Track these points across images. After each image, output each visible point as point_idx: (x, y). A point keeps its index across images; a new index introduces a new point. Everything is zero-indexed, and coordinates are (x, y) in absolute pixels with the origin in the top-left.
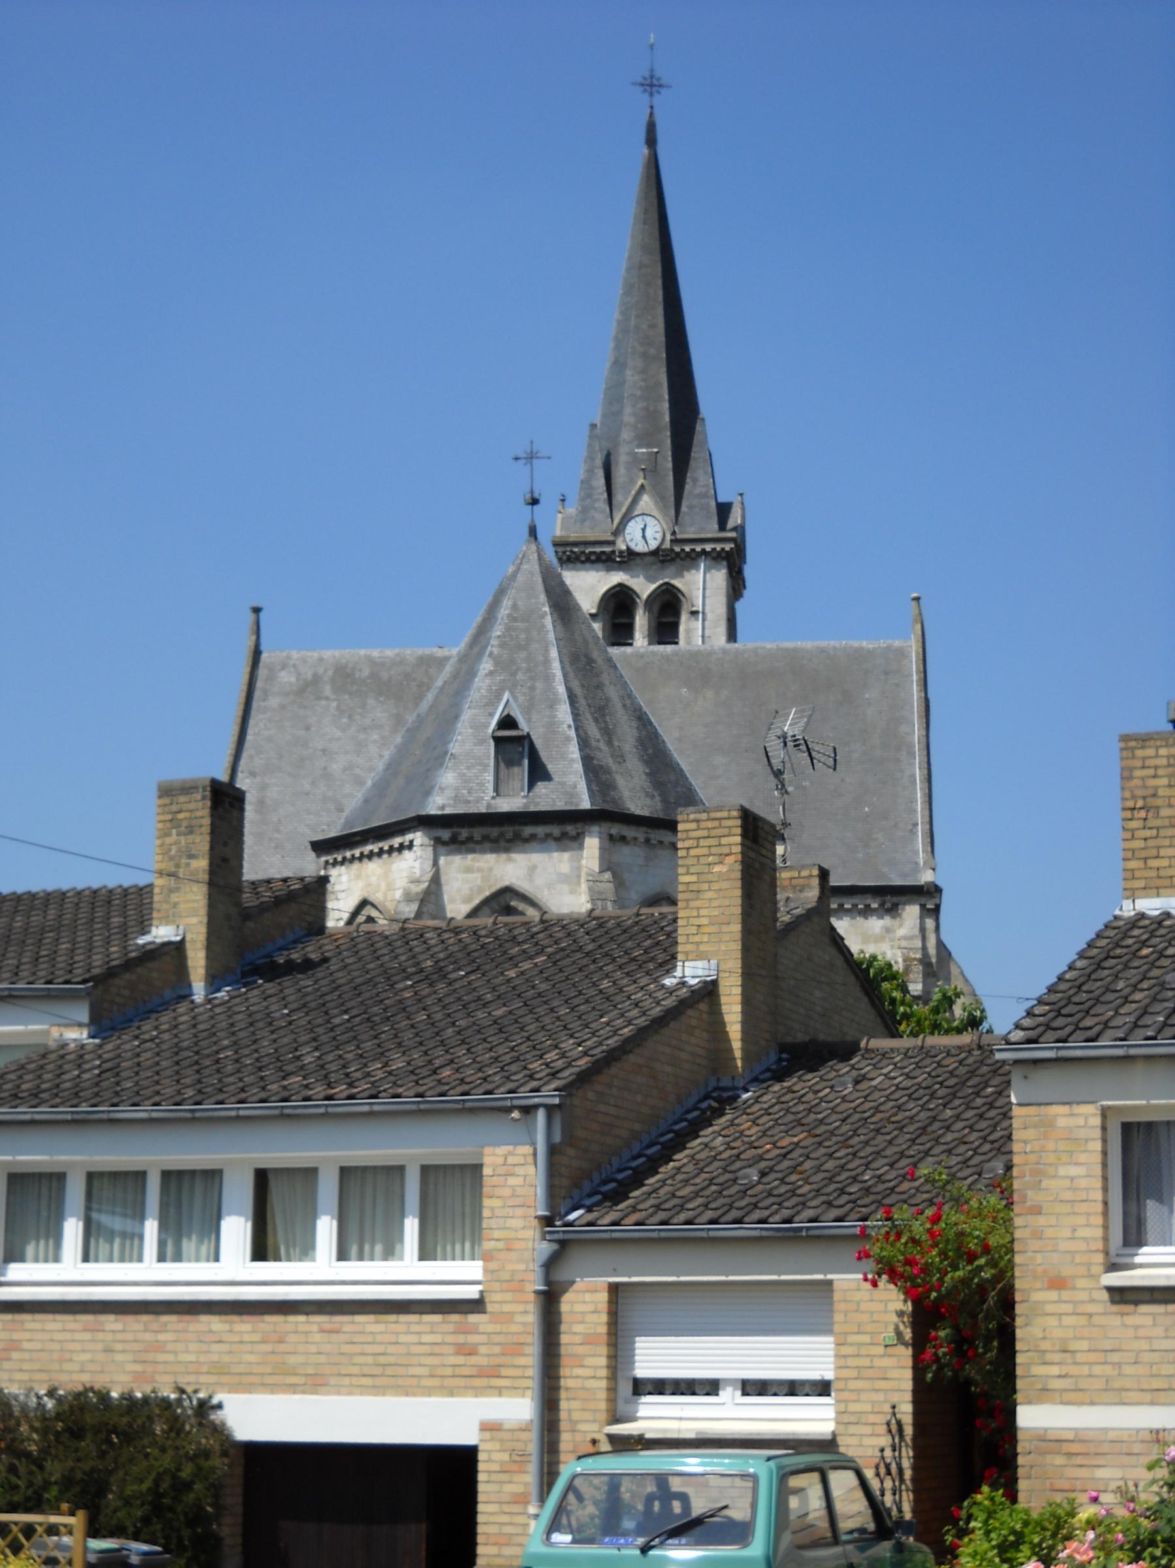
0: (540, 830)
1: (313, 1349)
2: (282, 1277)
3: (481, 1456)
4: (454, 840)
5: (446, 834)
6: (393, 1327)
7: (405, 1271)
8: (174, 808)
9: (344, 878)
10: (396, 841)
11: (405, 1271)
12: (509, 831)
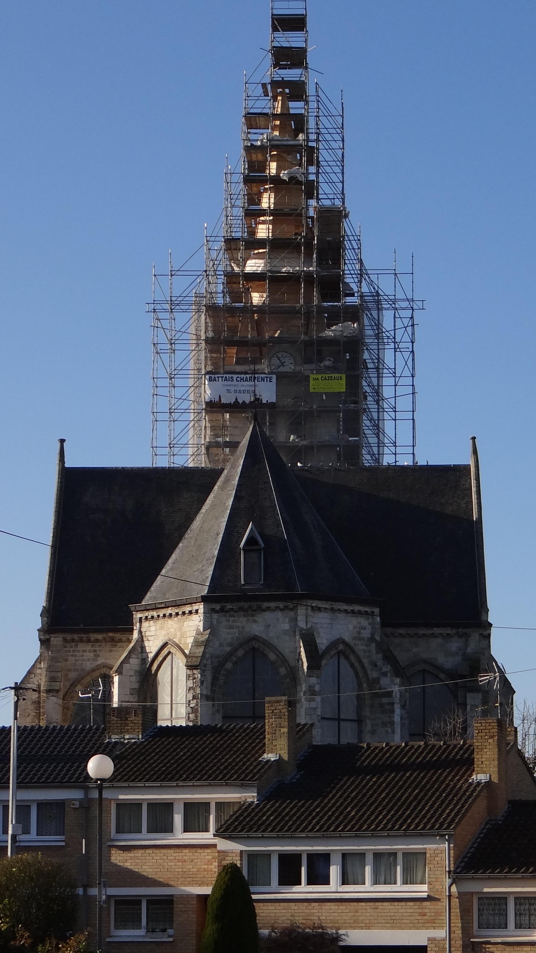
0: (272, 605)
1: (368, 914)
2: (352, 891)
3: (429, 949)
4: (222, 610)
5: (217, 607)
6: (397, 907)
7: (399, 889)
8: (273, 708)
9: (153, 628)
10: (187, 609)
11: (399, 889)
12: (254, 604)
